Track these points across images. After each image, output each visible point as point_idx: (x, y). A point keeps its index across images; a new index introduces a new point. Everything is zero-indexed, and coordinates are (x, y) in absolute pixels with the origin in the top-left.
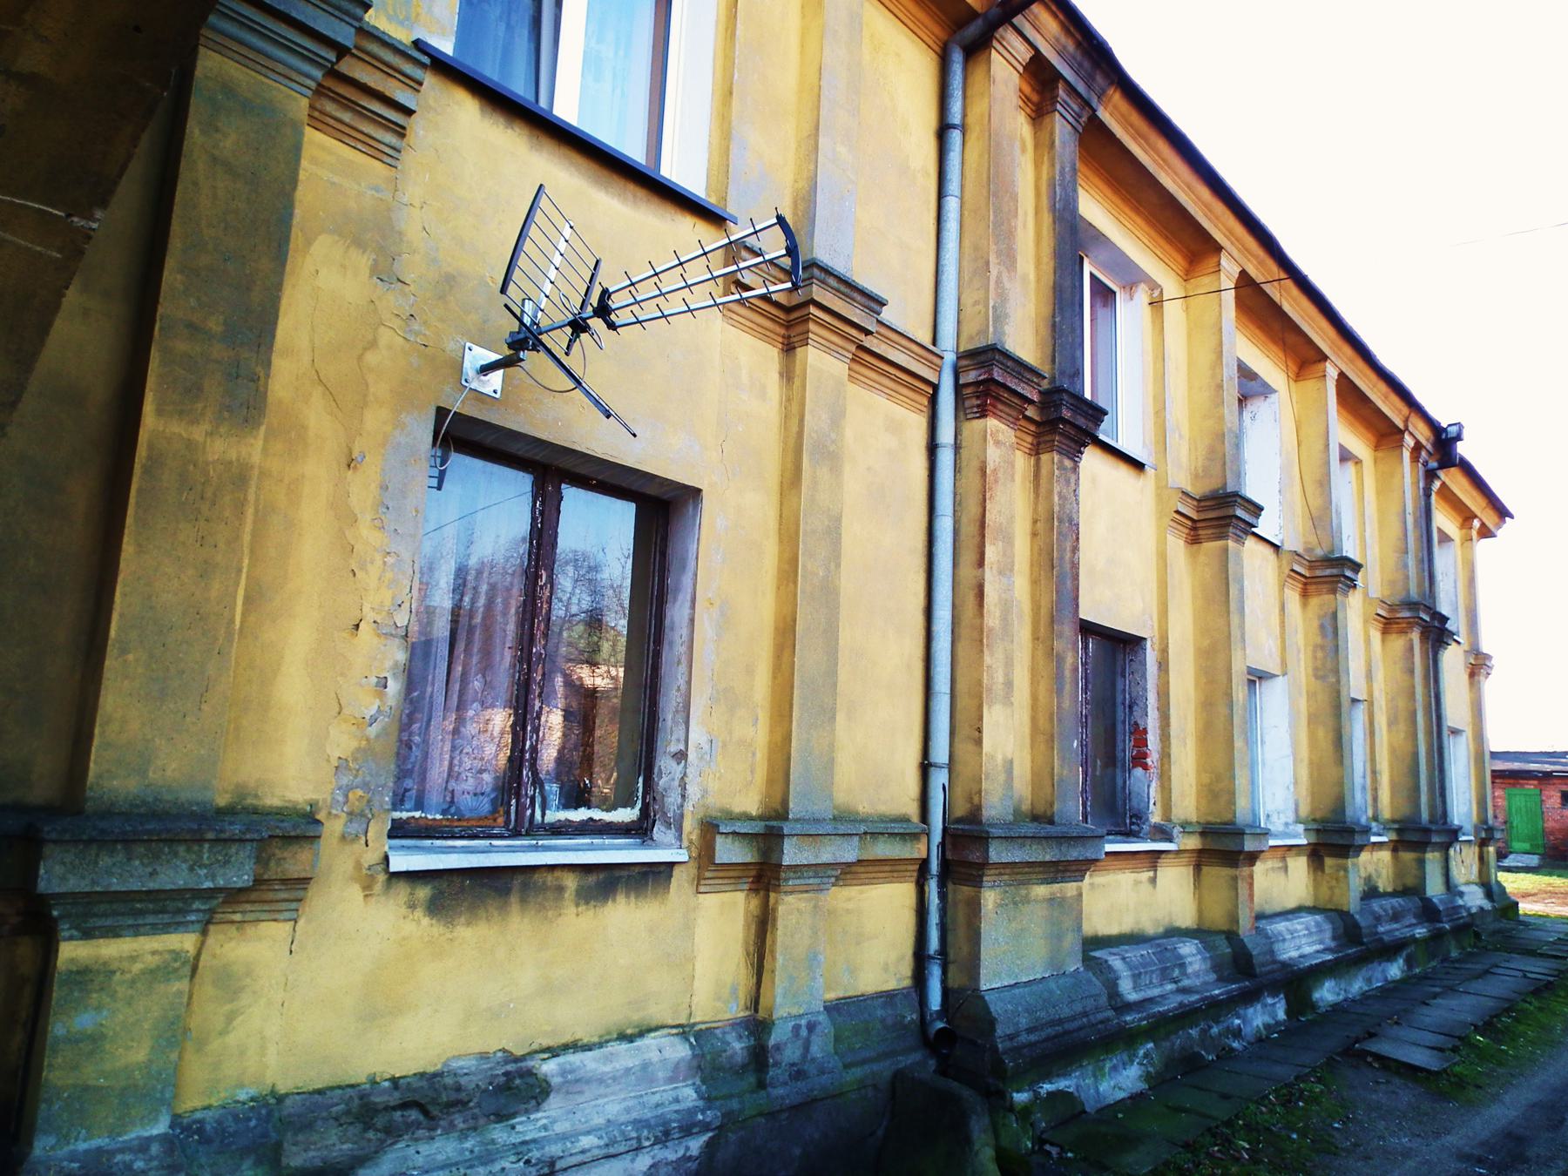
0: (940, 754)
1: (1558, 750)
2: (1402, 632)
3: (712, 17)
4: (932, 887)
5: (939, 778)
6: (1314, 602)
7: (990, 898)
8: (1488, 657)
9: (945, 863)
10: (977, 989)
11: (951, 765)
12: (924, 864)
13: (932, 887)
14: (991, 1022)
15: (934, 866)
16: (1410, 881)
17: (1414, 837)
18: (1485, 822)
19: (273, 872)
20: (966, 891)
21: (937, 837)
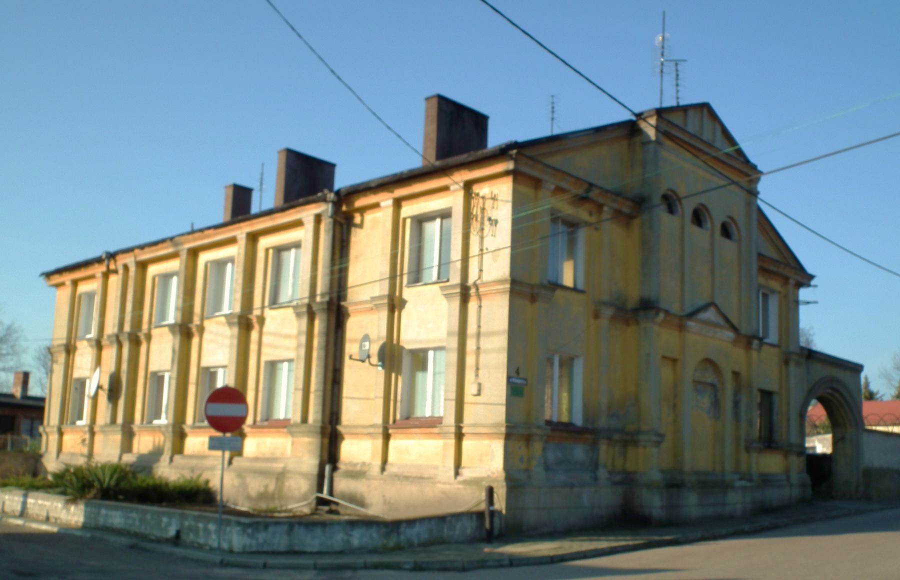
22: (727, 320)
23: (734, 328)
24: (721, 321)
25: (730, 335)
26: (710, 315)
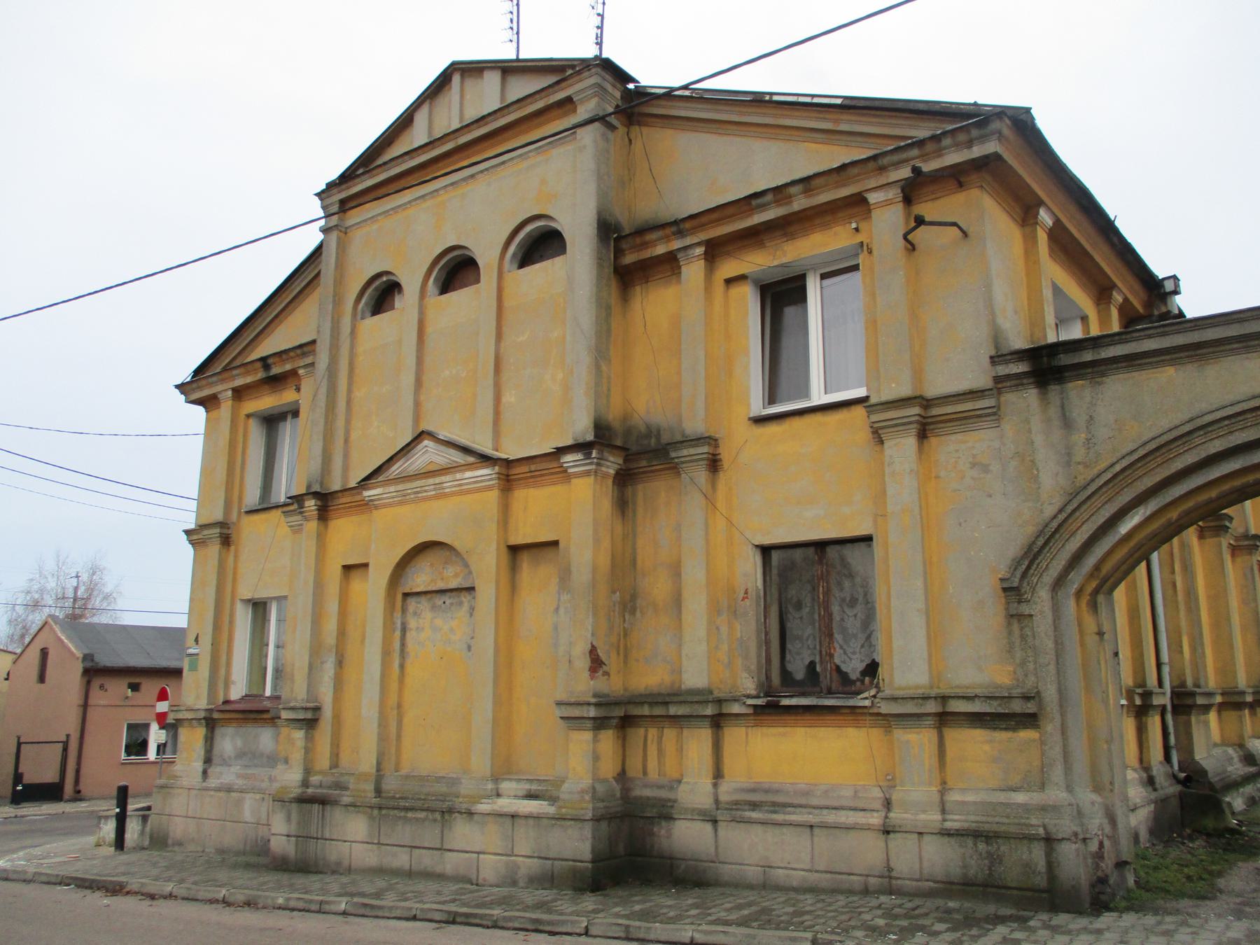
0: (1165, 657)
5: (1166, 670)
7: (1193, 719)
9: (1174, 707)
22: (466, 450)
24: (458, 457)
25: (486, 473)
26: (428, 454)
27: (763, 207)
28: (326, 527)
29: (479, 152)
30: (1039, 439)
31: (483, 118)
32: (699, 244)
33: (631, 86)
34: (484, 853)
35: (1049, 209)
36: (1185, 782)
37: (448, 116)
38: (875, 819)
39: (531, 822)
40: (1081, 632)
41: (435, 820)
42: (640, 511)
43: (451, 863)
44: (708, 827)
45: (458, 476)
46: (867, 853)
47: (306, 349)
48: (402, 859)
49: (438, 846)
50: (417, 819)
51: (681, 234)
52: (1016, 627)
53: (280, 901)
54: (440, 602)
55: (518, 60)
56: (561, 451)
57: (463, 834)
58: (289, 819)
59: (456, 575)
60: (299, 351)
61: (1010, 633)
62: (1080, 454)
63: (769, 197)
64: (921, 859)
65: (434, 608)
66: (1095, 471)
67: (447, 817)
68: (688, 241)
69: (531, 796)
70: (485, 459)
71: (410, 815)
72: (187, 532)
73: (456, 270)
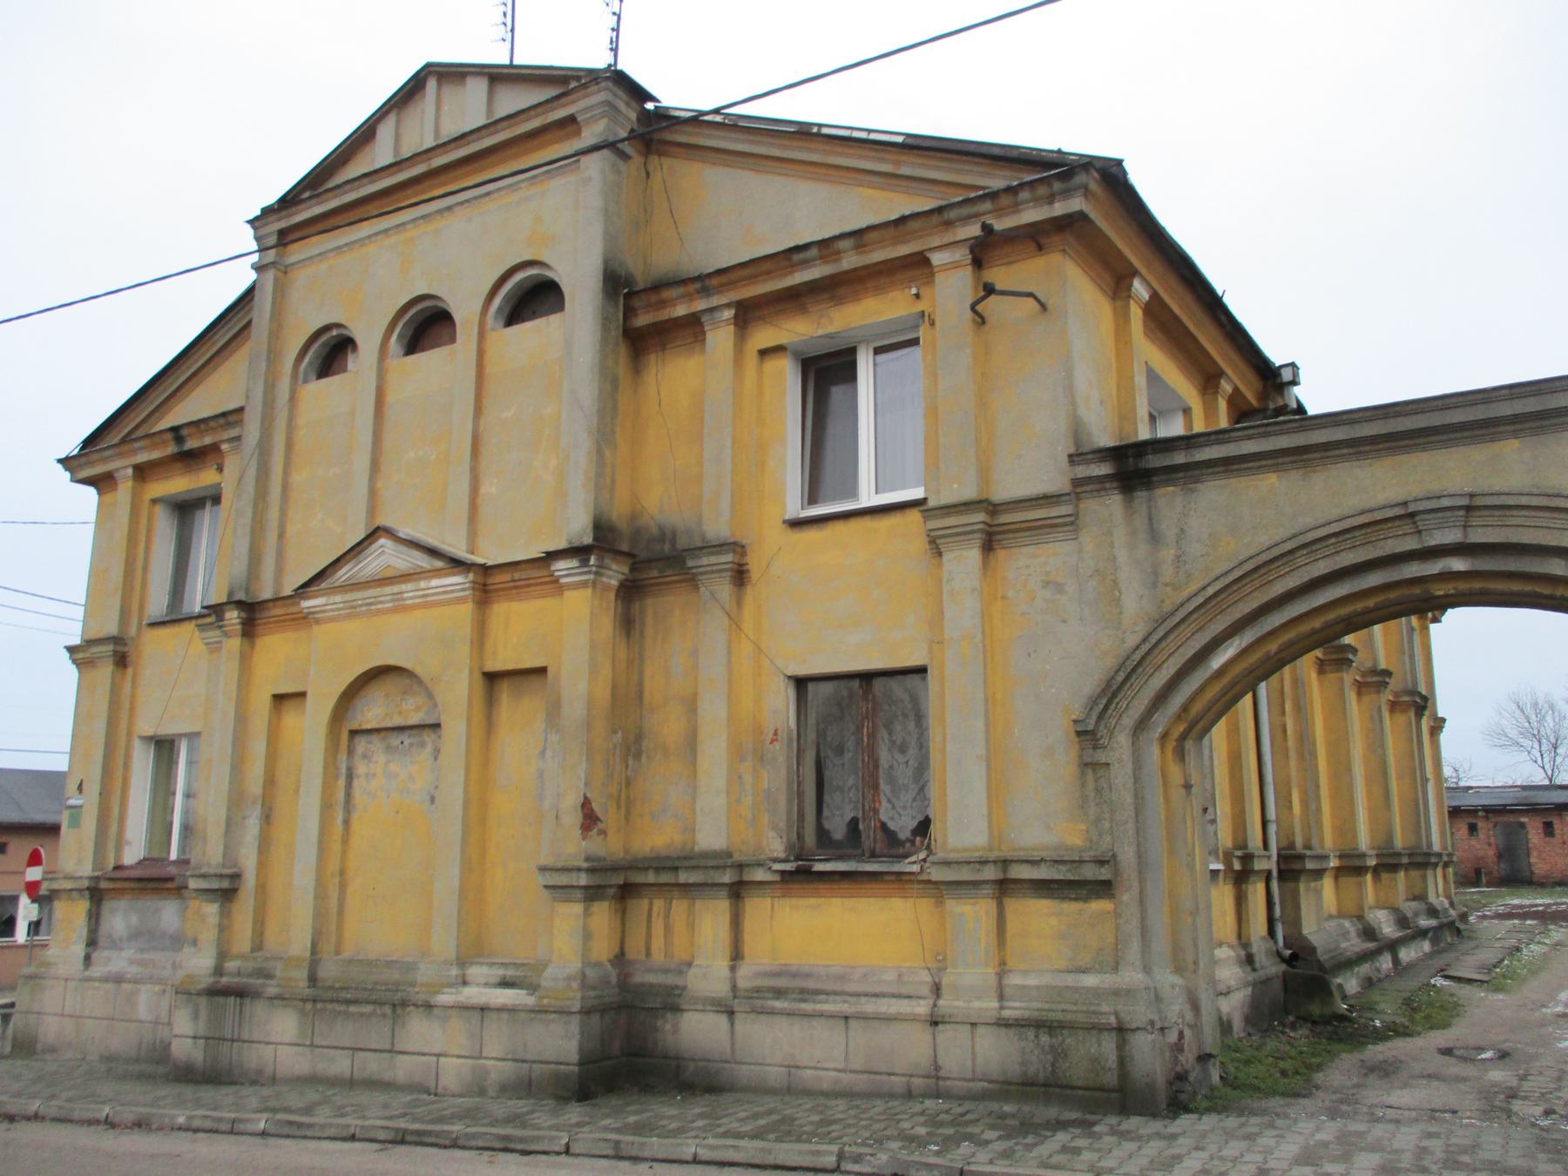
0: (1272, 814)
1: (801, 242)
2: (1404, 711)
3: (1264, 539)
4: (1275, 885)
5: (1272, 828)
6: (1366, 699)
7: (1302, 887)
8: (1443, 720)
9: (1280, 872)
10: (1300, 933)
11: (1278, 821)
12: (1269, 872)
13: (1275, 885)
14: (1314, 949)
15: (1275, 873)
16: (1417, 891)
17: (1420, 859)
18: (1244, 846)
19: (746, 878)
20: (1291, 885)
21: (1275, 858)
22: (433, 552)
23: (457, 564)
24: (424, 561)
26: (384, 557)
27: (806, 263)
28: (253, 646)
29: (423, 192)
30: (1122, 556)
31: (463, 136)
32: (728, 305)
33: (650, 106)
34: (445, 1055)
35: (1144, 280)
36: (1292, 960)
37: (420, 131)
38: (922, 1008)
39: (505, 1016)
40: (1165, 784)
41: (384, 1015)
42: (649, 631)
43: (403, 1069)
44: (723, 1020)
45: (423, 584)
46: (909, 1049)
47: (231, 419)
48: (341, 1065)
49: (388, 1046)
50: (361, 1015)
51: (706, 292)
52: (1090, 777)
53: (181, 1120)
54: (397, 742)
55: (511, 66)
56: (552, 556)
57: (420, 1032)
58: (196, 1017)
59: (418, 709)
60: (222, 421)
61: (1083, 785)
62: (1168, 573)
63: (814, 252)
64: (973, 1054)
65: (389, 749)
66: (1185, 594)
67: (399, 1011)
68: (715, 301)
69: (505, 984)
70: (457, 564)
71: (352, 1009)
72: (71, 650)
73: (426, 325)
